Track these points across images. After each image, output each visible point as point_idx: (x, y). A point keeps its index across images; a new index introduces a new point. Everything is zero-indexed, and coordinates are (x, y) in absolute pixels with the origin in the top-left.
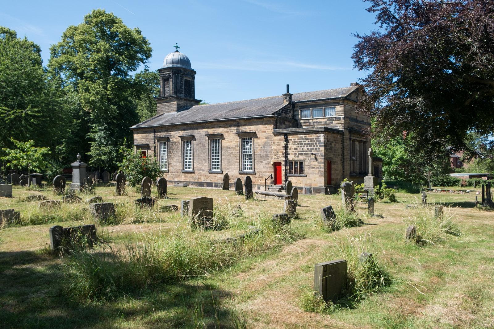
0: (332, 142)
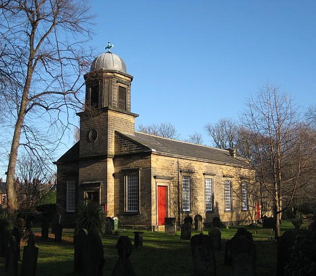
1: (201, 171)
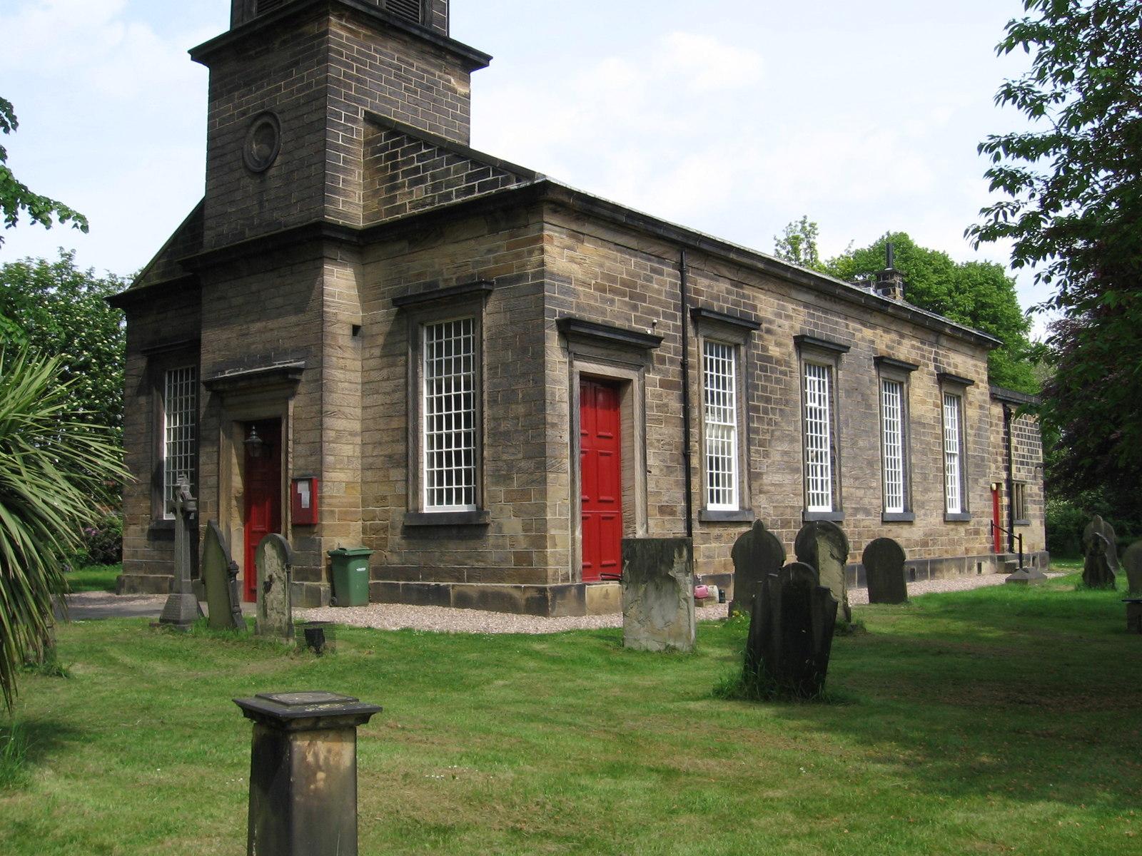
1: (786, 323)
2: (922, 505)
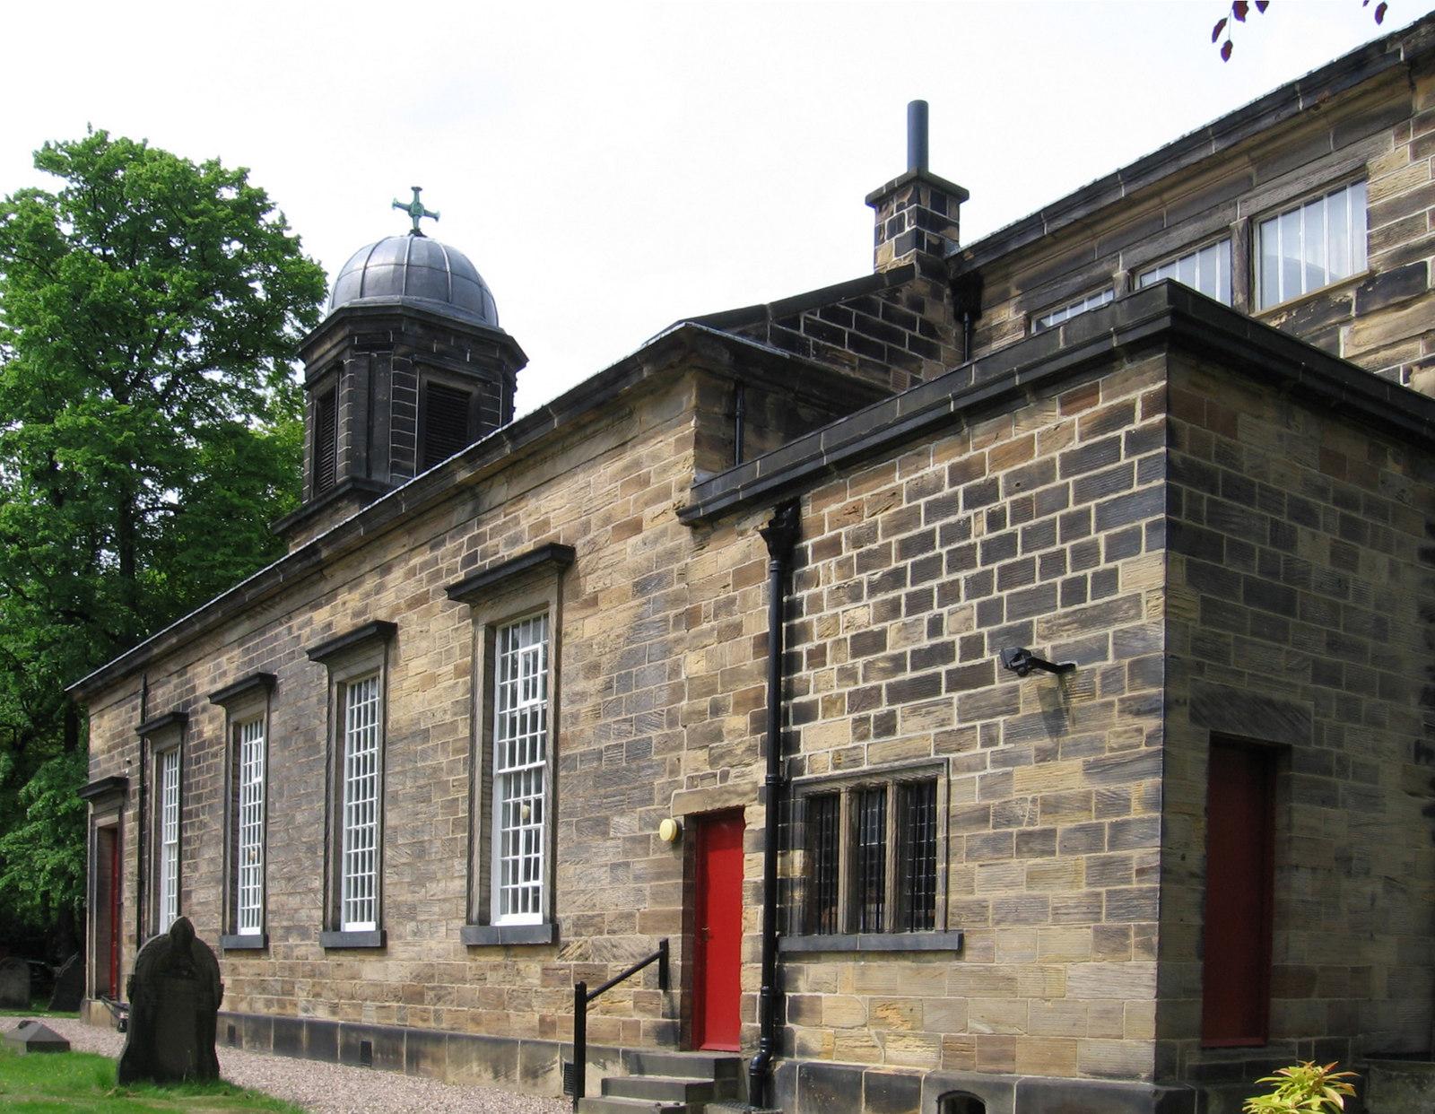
0: (1305, 514)
2: (411, 913)
